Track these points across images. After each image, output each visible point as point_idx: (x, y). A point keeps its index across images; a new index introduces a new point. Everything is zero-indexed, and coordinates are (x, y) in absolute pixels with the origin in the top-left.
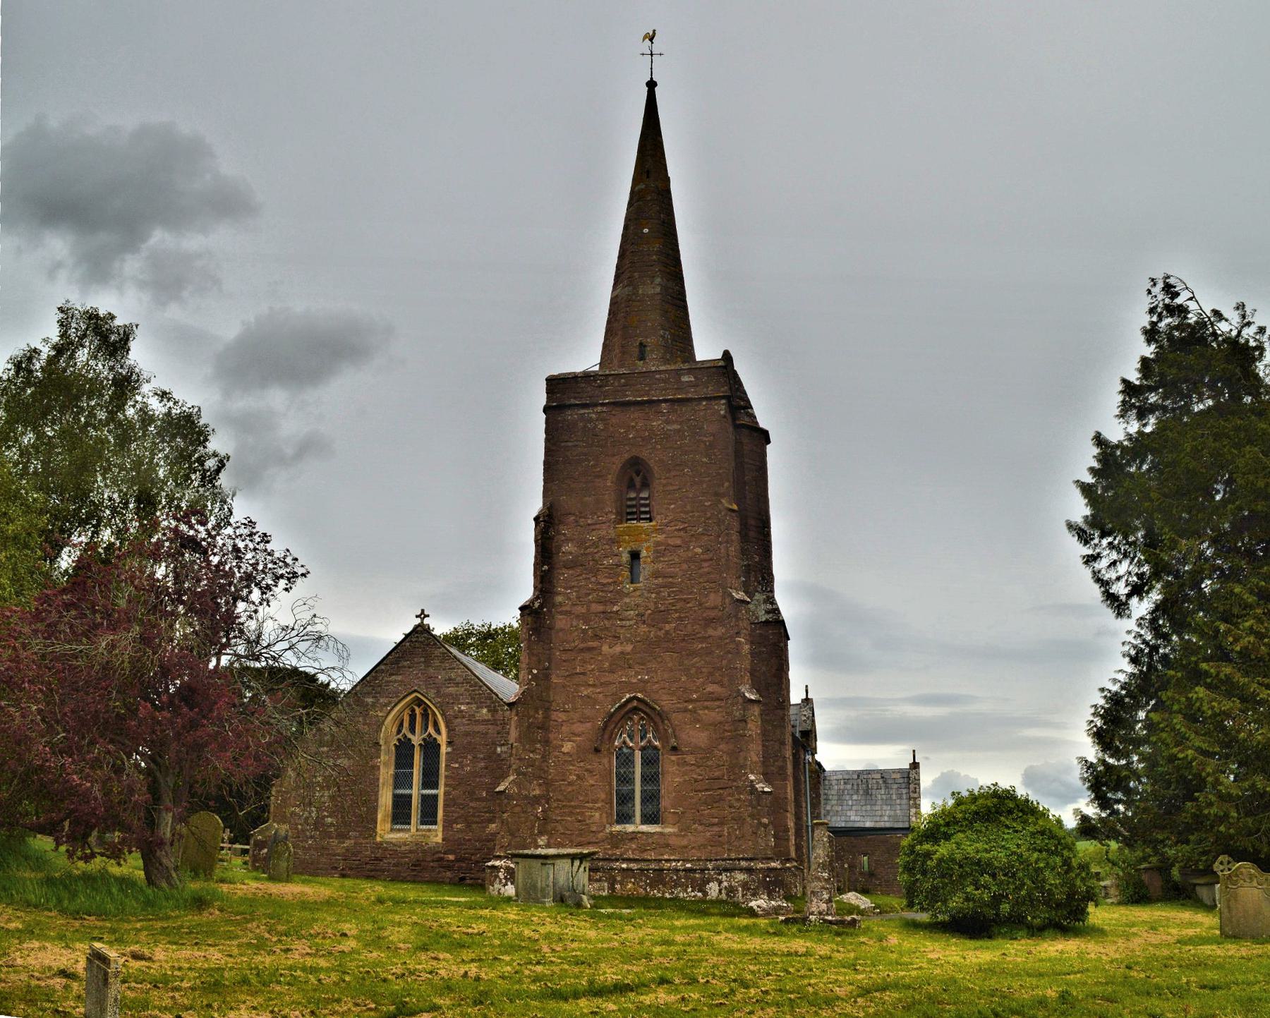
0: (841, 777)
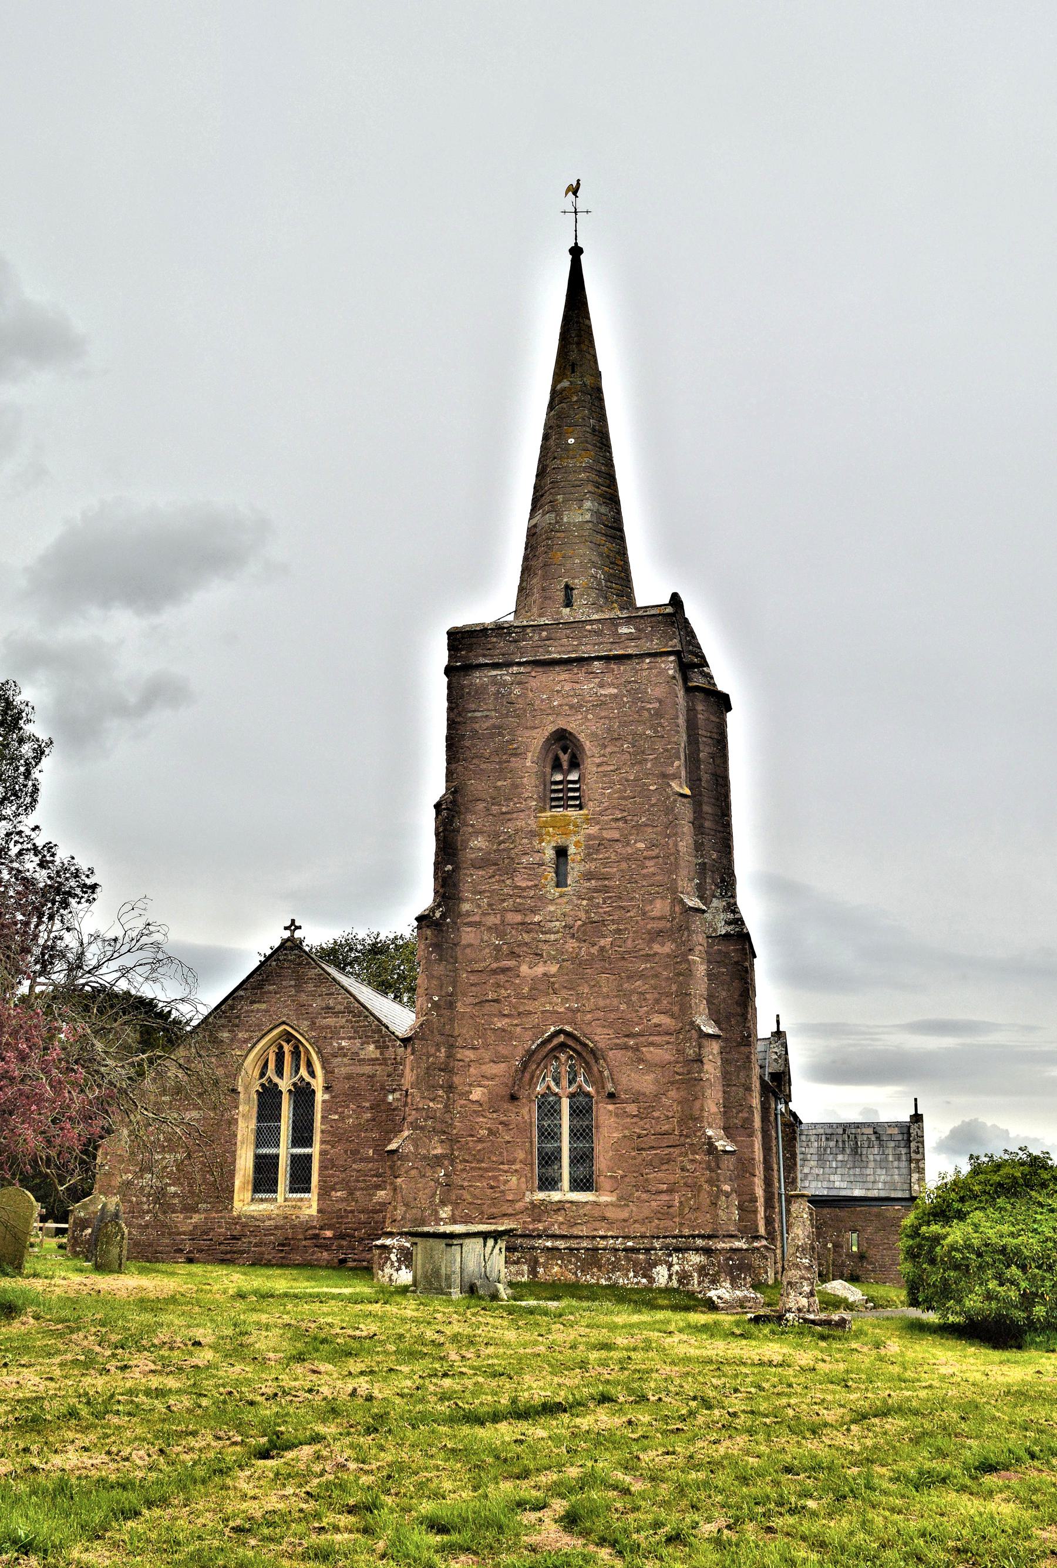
0: (821, 1131)
